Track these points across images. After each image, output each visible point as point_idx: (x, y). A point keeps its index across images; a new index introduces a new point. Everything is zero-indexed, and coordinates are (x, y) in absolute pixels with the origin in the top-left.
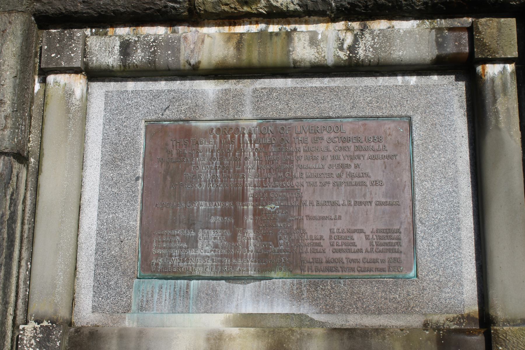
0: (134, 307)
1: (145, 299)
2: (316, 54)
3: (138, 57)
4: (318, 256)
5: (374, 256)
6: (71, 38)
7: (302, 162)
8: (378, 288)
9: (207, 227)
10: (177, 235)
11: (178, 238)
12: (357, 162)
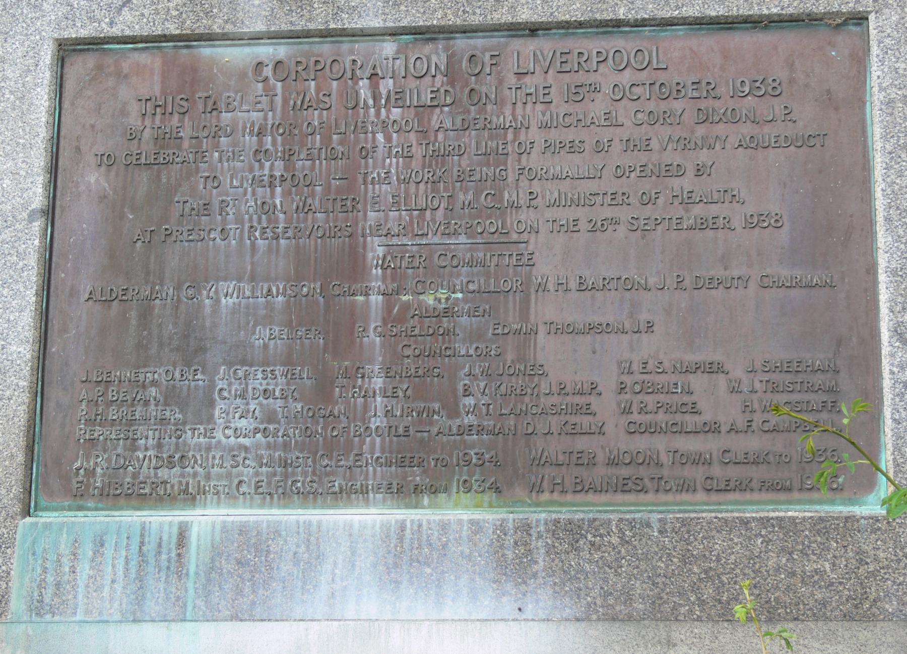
1: (50, 579)
4: (582, 443)
5: (754, 443)
7: (534, 161)
8: (767, 542)
9: (241, 358)
10: (154, 383)
11: (153, 391)
12: (704, 156)
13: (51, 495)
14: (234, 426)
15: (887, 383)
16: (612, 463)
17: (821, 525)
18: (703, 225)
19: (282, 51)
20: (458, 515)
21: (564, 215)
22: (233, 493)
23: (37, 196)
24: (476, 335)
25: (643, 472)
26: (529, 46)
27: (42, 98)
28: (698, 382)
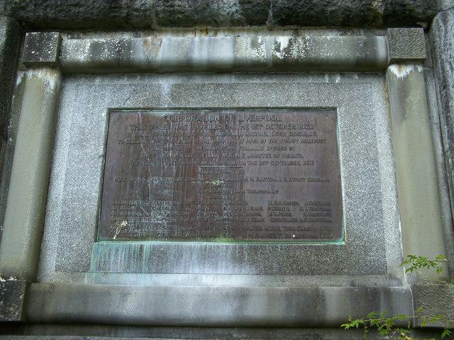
0: (93, 267)
1: (102, 260)
2: (257, 54)
3: (106, 55)
4: (257, 224)
5: (307, 225)
6: (49, 39)
7: (244, 145)
8: (311, 252)
10: (134, 205)
11: (133, 207)
12: (292, 145)
13: (103, 236)
14: (158, 217)
15: (344, 208)
16: (266, 230)
17: (326, 248)
18: (292, 164)
19: (172, 113)
20: (222, 244)
21: (253, 160)
22: (156, 237)
23: (101, 151)
24: (227, 193)
25: (275, 232)
26: (243, 114)
27: (104, 125)
28: (291, 207)
